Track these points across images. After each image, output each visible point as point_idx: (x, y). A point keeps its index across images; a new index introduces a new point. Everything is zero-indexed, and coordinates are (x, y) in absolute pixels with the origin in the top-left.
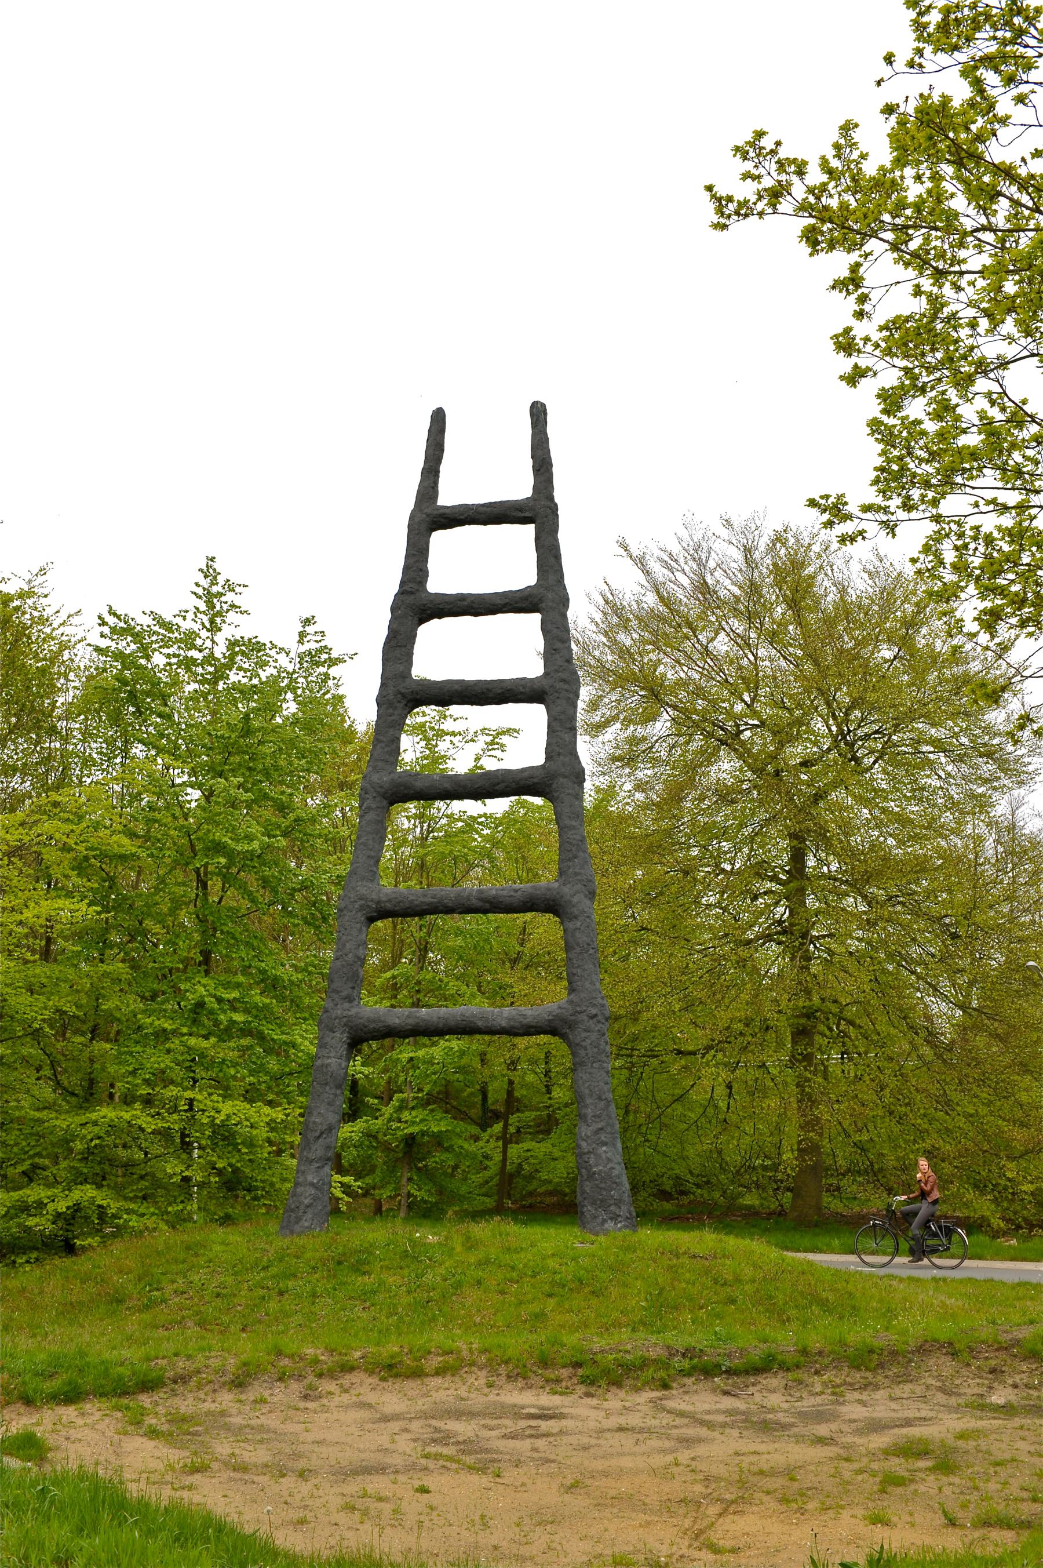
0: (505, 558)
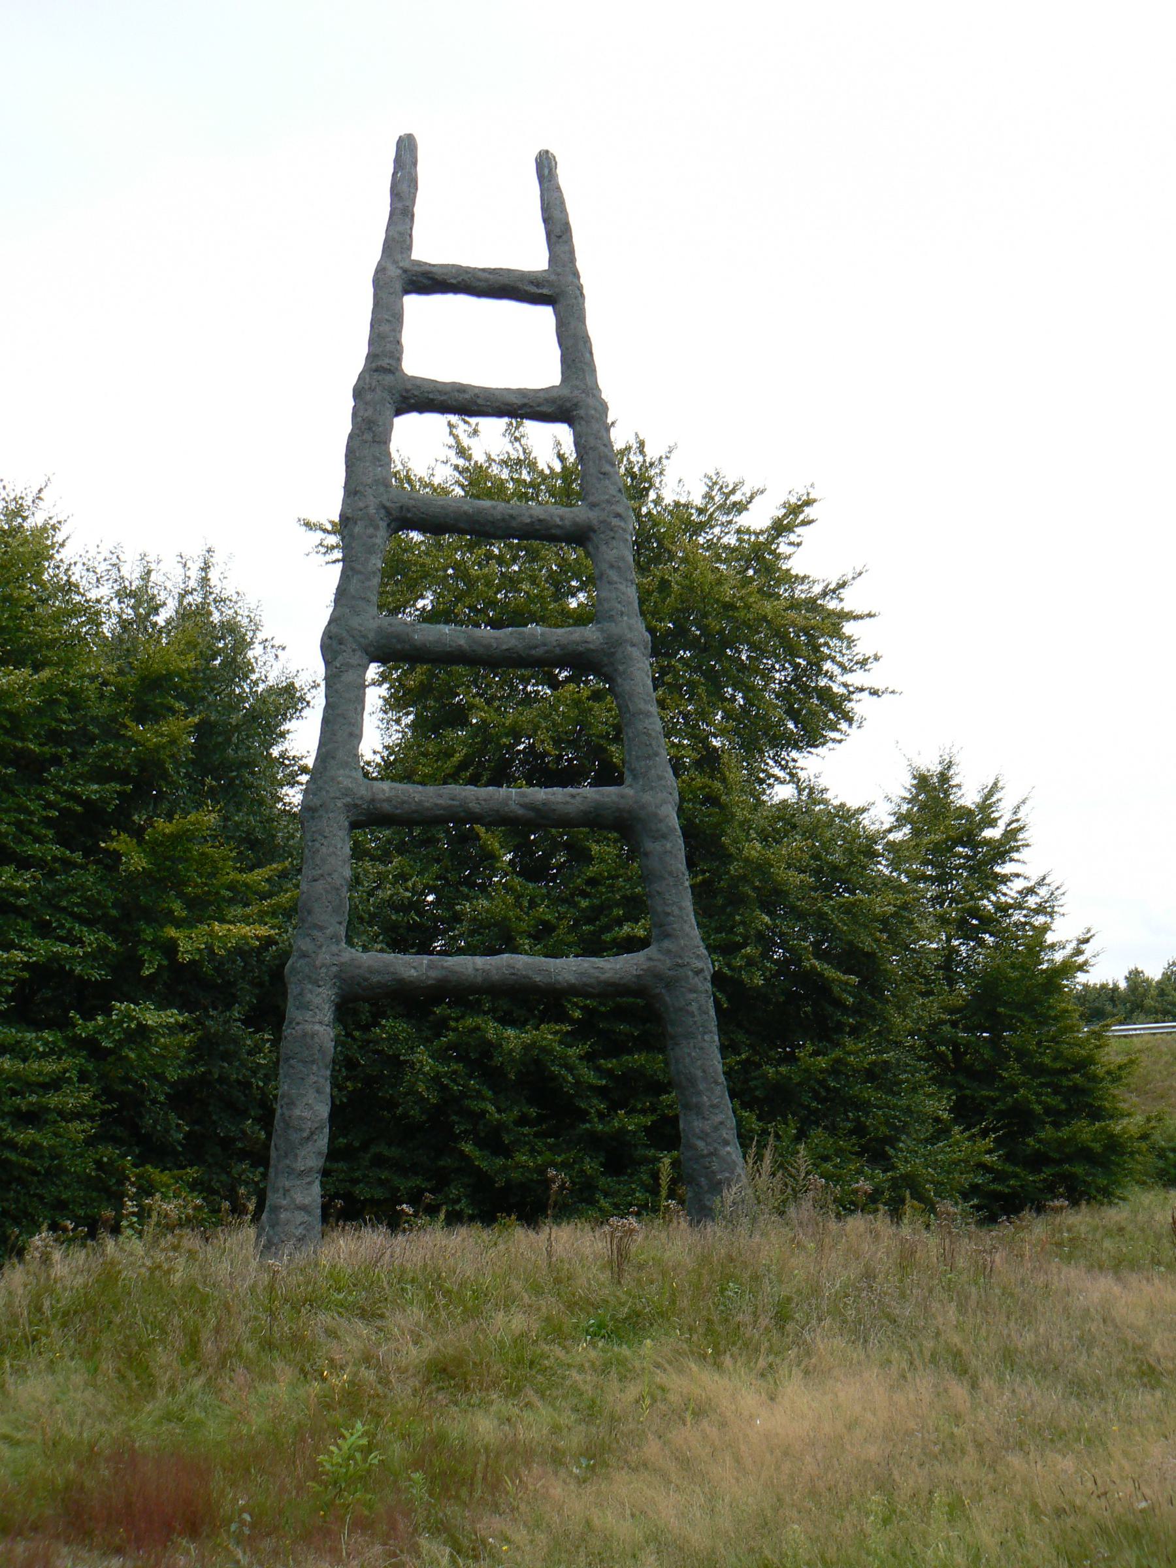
0: (512, 348)
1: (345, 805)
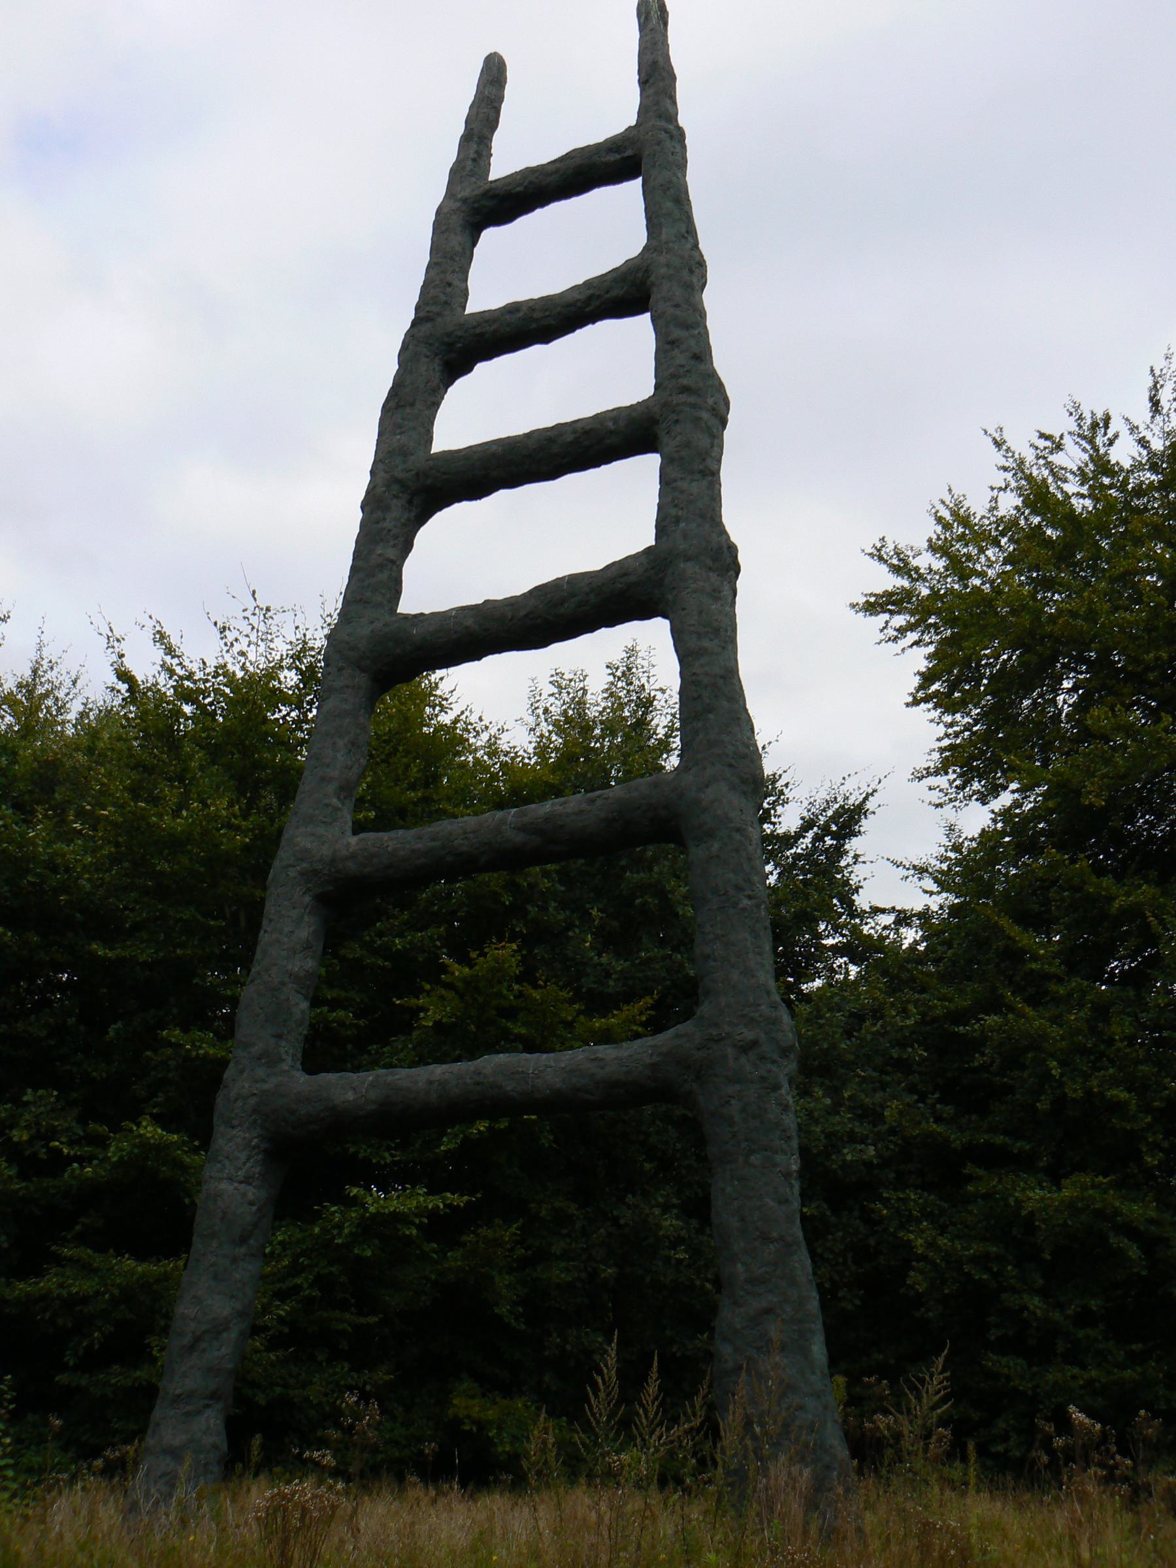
1: (302, 874)
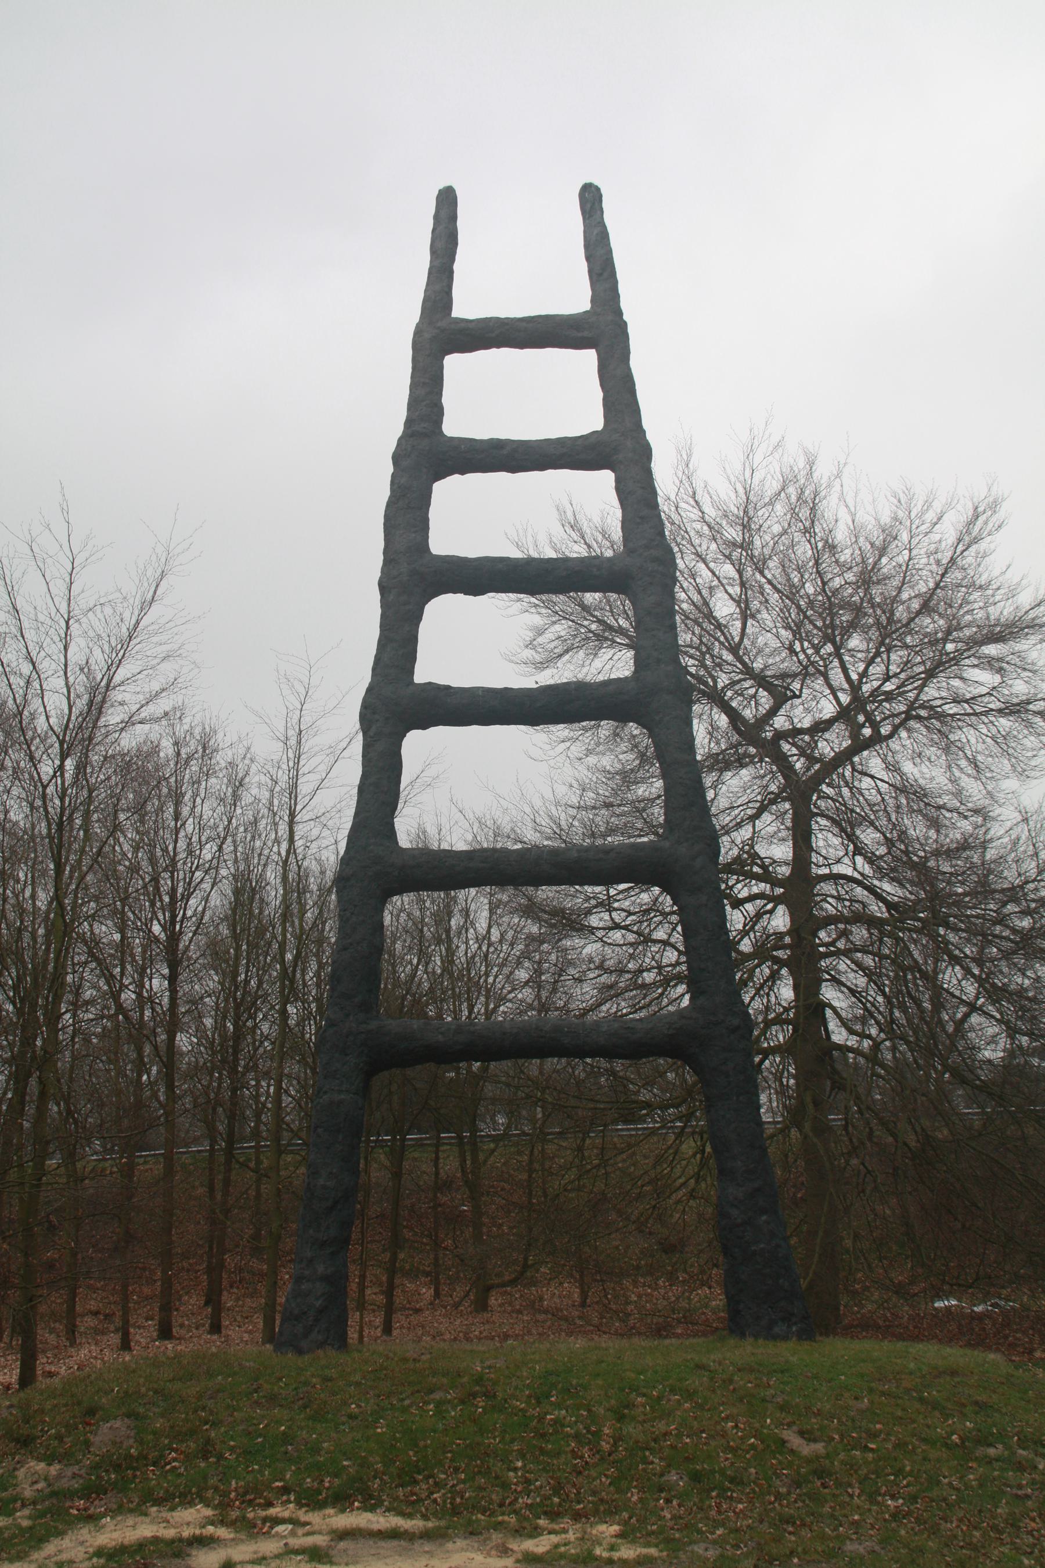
0: (562, 395)
